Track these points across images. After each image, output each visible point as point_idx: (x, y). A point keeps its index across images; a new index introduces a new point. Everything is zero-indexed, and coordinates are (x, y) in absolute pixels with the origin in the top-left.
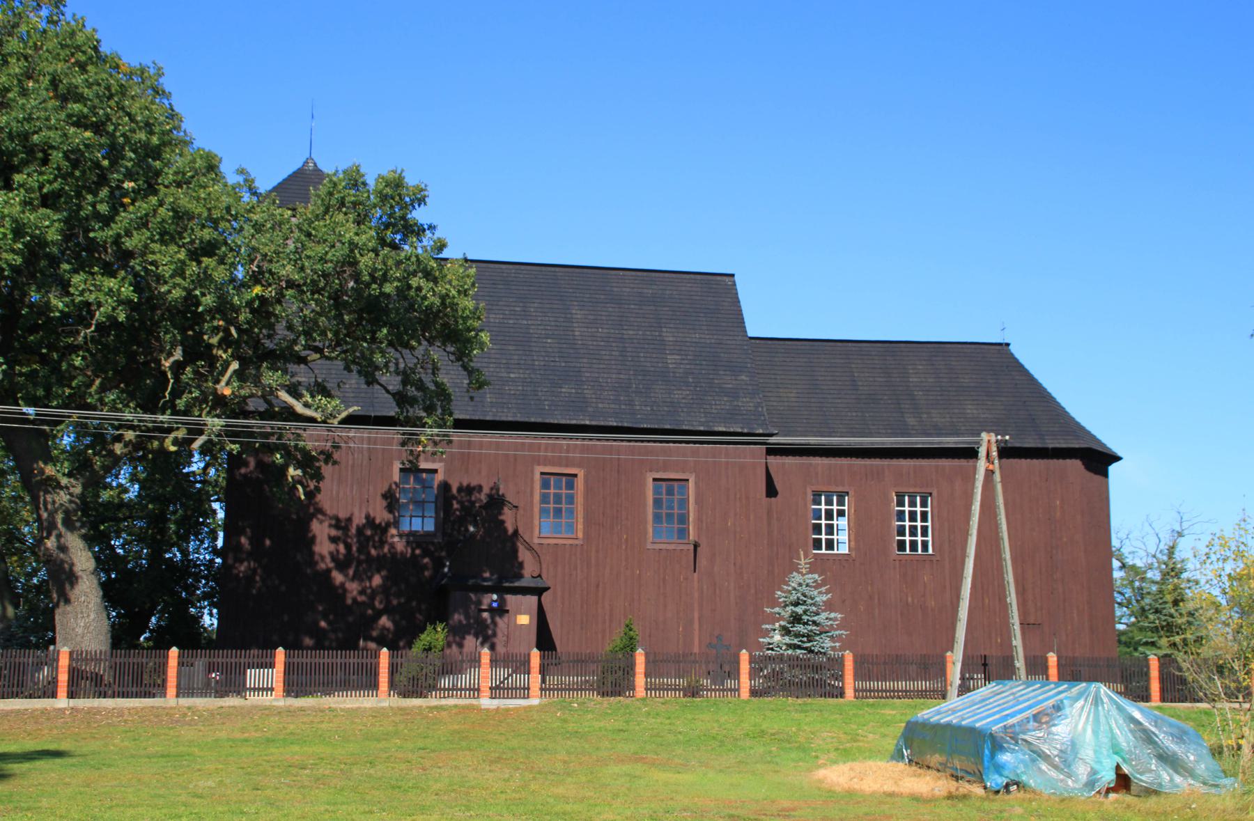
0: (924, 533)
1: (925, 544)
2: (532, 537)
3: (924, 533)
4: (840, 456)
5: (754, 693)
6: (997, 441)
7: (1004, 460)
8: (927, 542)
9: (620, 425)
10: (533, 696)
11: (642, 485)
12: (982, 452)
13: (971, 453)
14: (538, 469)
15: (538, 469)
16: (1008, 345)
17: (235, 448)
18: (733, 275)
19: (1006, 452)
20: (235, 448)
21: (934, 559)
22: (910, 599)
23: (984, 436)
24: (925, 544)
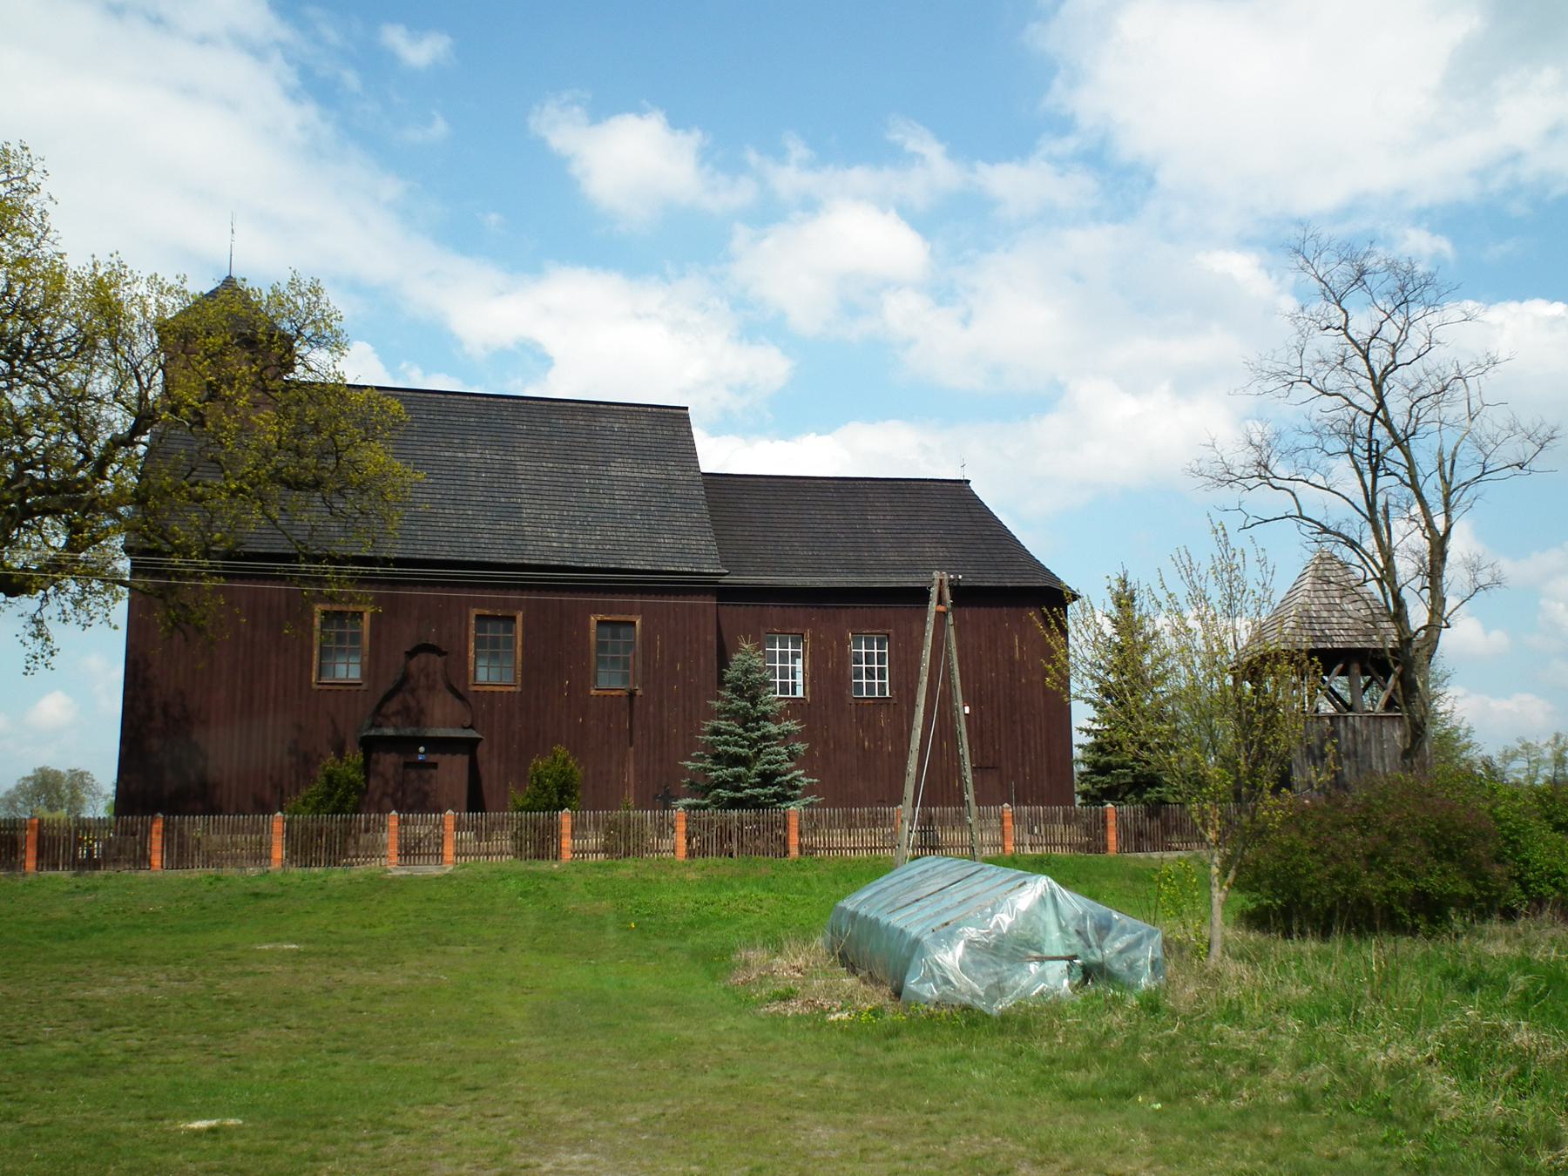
0: (882, 676)
1: (882, 686)
2: (466, 685)
3: (882, 676)
4: (603, 568)
5: (691, 854)
6: (950, 580)
7: (967, 612)
8: (884, 684)
9: (562, 563)
10: (447, 862)
11: (587, 628)
12: (934, 591)
13: (921, 595)
14: (474, 612)
15: (474, 612)
16: (968, 481)
17: (1375, 637)
18: (687, 408)
19: (963, 595)
20: (1375, 637)
21: (892, 702)
22: (866, 744)
23: (936, 575)
24: (882, 686)
